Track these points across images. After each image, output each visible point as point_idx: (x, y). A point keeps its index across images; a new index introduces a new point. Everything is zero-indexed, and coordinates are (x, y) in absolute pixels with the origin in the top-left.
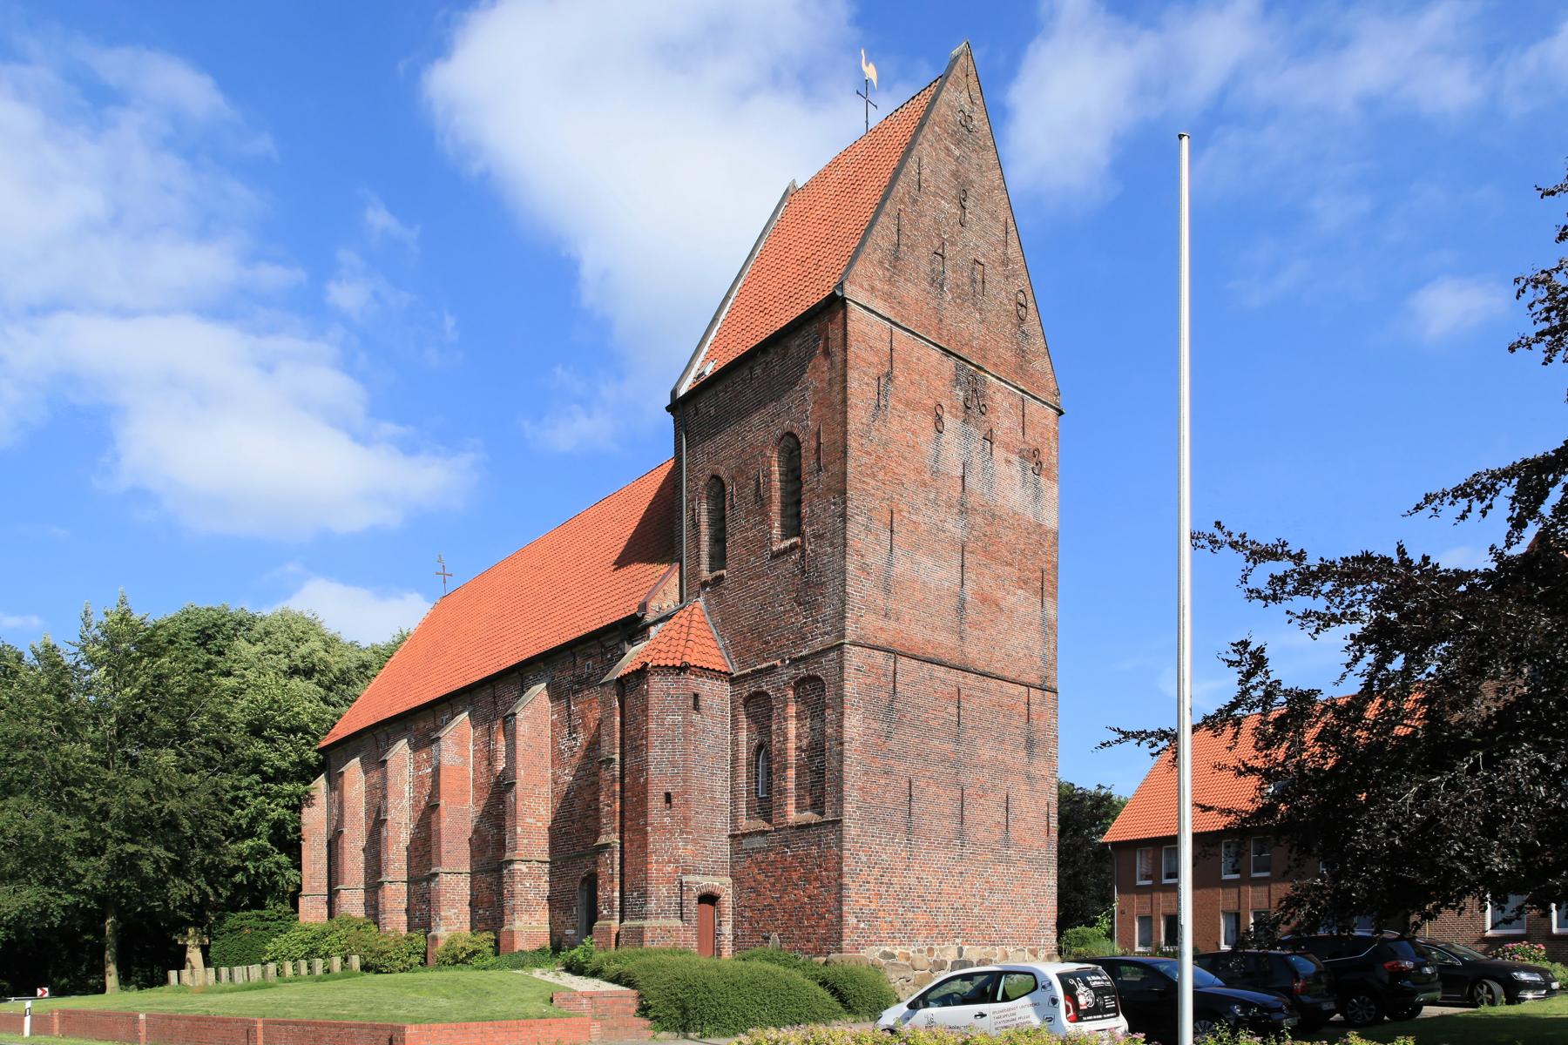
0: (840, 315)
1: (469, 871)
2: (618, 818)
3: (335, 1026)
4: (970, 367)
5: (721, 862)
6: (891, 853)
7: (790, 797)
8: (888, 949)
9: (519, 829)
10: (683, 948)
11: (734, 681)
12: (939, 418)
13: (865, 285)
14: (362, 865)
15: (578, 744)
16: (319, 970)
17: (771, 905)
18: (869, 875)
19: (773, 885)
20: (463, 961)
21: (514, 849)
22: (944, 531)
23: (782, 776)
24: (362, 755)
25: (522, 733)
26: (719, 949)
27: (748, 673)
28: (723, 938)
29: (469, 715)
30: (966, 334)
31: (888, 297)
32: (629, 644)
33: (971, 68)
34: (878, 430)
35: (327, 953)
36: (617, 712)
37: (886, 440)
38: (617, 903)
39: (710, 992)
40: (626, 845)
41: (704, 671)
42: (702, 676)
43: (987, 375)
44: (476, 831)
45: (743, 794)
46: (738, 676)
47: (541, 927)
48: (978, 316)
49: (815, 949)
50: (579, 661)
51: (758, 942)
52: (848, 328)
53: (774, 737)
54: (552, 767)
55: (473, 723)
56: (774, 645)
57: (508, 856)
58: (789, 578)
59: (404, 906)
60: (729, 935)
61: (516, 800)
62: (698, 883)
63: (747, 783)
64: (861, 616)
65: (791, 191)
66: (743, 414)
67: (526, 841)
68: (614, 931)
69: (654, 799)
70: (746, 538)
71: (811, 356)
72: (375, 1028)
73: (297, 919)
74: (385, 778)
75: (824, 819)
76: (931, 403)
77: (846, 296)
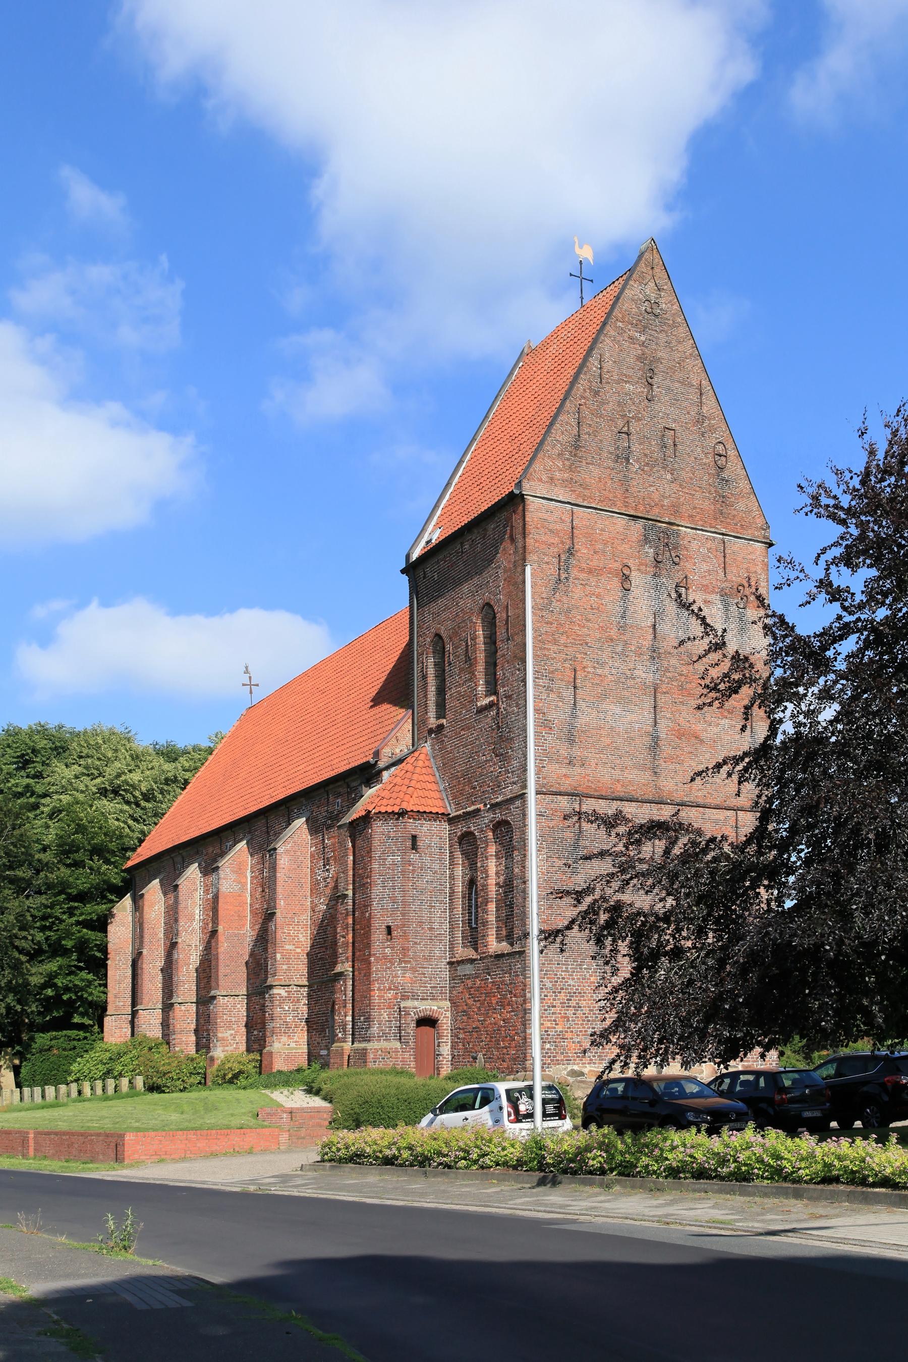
0: (521, 508)
1: (246, 993)
2: (350, 948)
3: (82, 1134)
4: (660, 524)
5: (440, 987)
6: (578, 979)
7: (491, 928)
8: (576, 1068)
9: (278, 956)
10: (401, 1068)
11: (452, 821)
12: (626, 578)
13: (544, 478)
14: (160, 985)
15: (331, 876)
16: (110, 1090)
17: (479, 1028)
18: (554, 1000)
19: (479, 1009)
20: (230, 1082)
21: (274, 975)
22: (634, 679)
23: (484, 909)
24: (162, 876)
25: (282, 866)
26: (438, 1068)
27: (460, 815)
28: (441, 1058)
29: (247, 843)
30: (656, 496)
31: (569, 483)
32: (366, 787)
33: (657, 260)
34: (560, 601)
35: (121, 1073)
36: (350, 852)
37: (569, 608)
38: (350, 1026)
39: (382, 1107)
40: (356, 973)
41: (421, 814)
42: (419, 819)
43: (680, 528)
44: (252, 955)
45: (459, 924)
46: (453, 817)
47: (299, 1048)
48: (669, 476)
49: (508, 1068)
50: (331, 798)
51: (468, 1062)
52: (527, 519)
53: (479, 873)
54: (311, 896)
55: (251, 851)
56: (480, 790)
57: (270, 981)
58: (489, 731)
59: (193, 1026)
60: (448, 1055)
61: (276, 928)
62: (415, 1008)
63: (462, 914)
64: (544, 767)
65: (526, 351)
66: (457, 583)
67: (285, 967)
68: (347, 1053)
69: (376, 932)
70: (459, 692)
71: (502, 540)
72: (107, 1135)
73: (102, 1039)
74: (176, 898)
75: (514, 950)
76: (617, 566)
77: (524, 493)
